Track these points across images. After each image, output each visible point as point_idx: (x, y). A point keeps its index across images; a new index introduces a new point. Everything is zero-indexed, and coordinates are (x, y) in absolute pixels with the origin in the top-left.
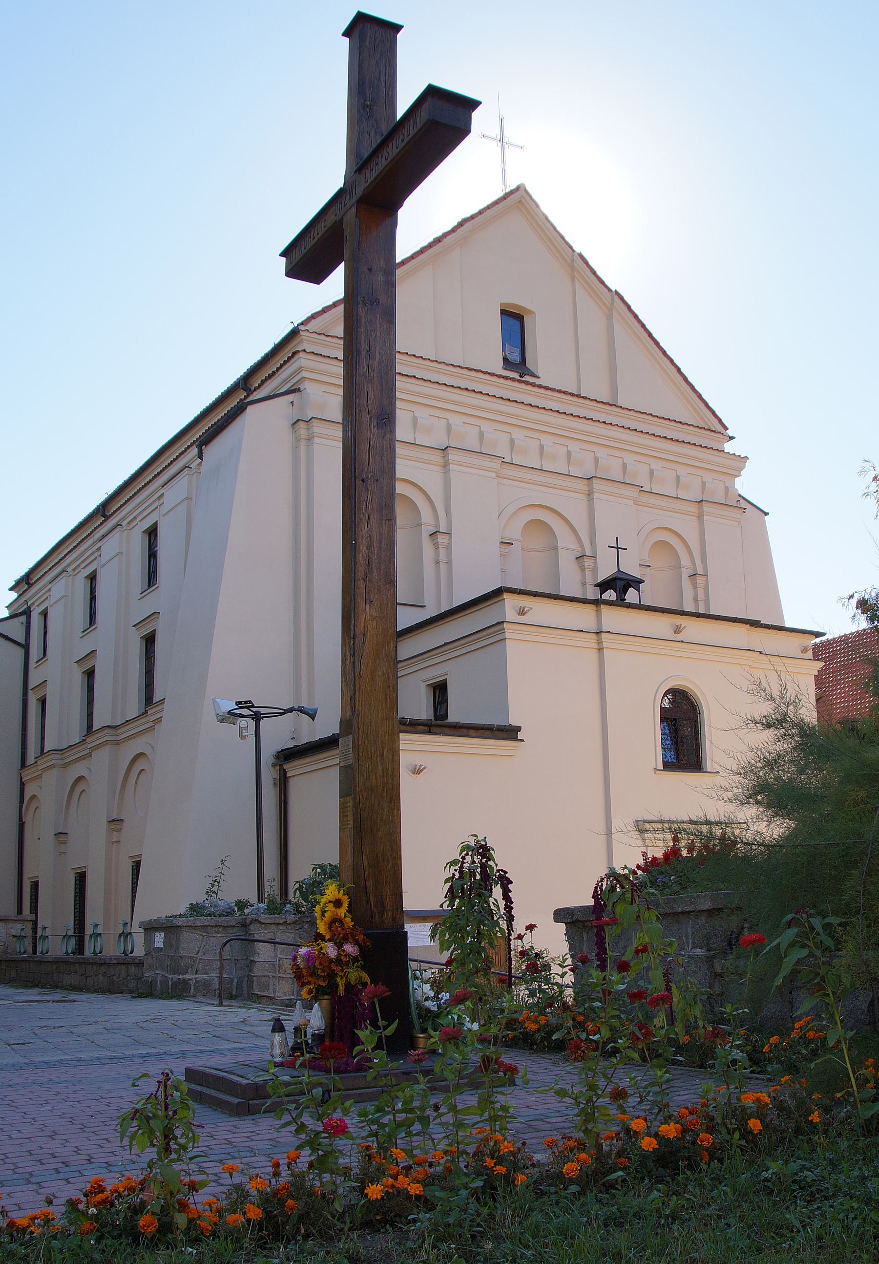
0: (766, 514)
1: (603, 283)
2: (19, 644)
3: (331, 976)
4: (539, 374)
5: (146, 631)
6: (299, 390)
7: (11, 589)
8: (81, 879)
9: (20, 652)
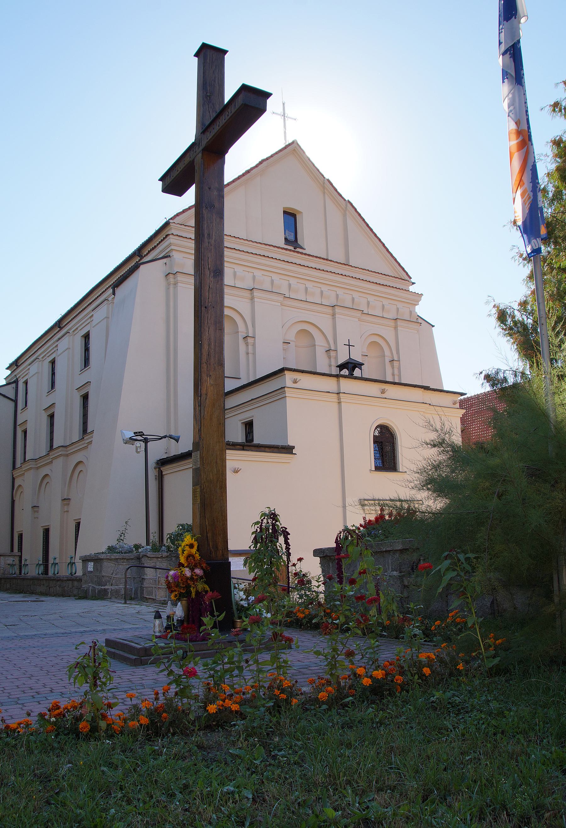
0: (433, 326)
1: (341, 196)
2: (11, 400)
3: (188, 587)
4: (305, 247)
5: (83, 392)
6: (169, 256)
7: (7, 369)
8: (47, 532)
9: (12, 404)
